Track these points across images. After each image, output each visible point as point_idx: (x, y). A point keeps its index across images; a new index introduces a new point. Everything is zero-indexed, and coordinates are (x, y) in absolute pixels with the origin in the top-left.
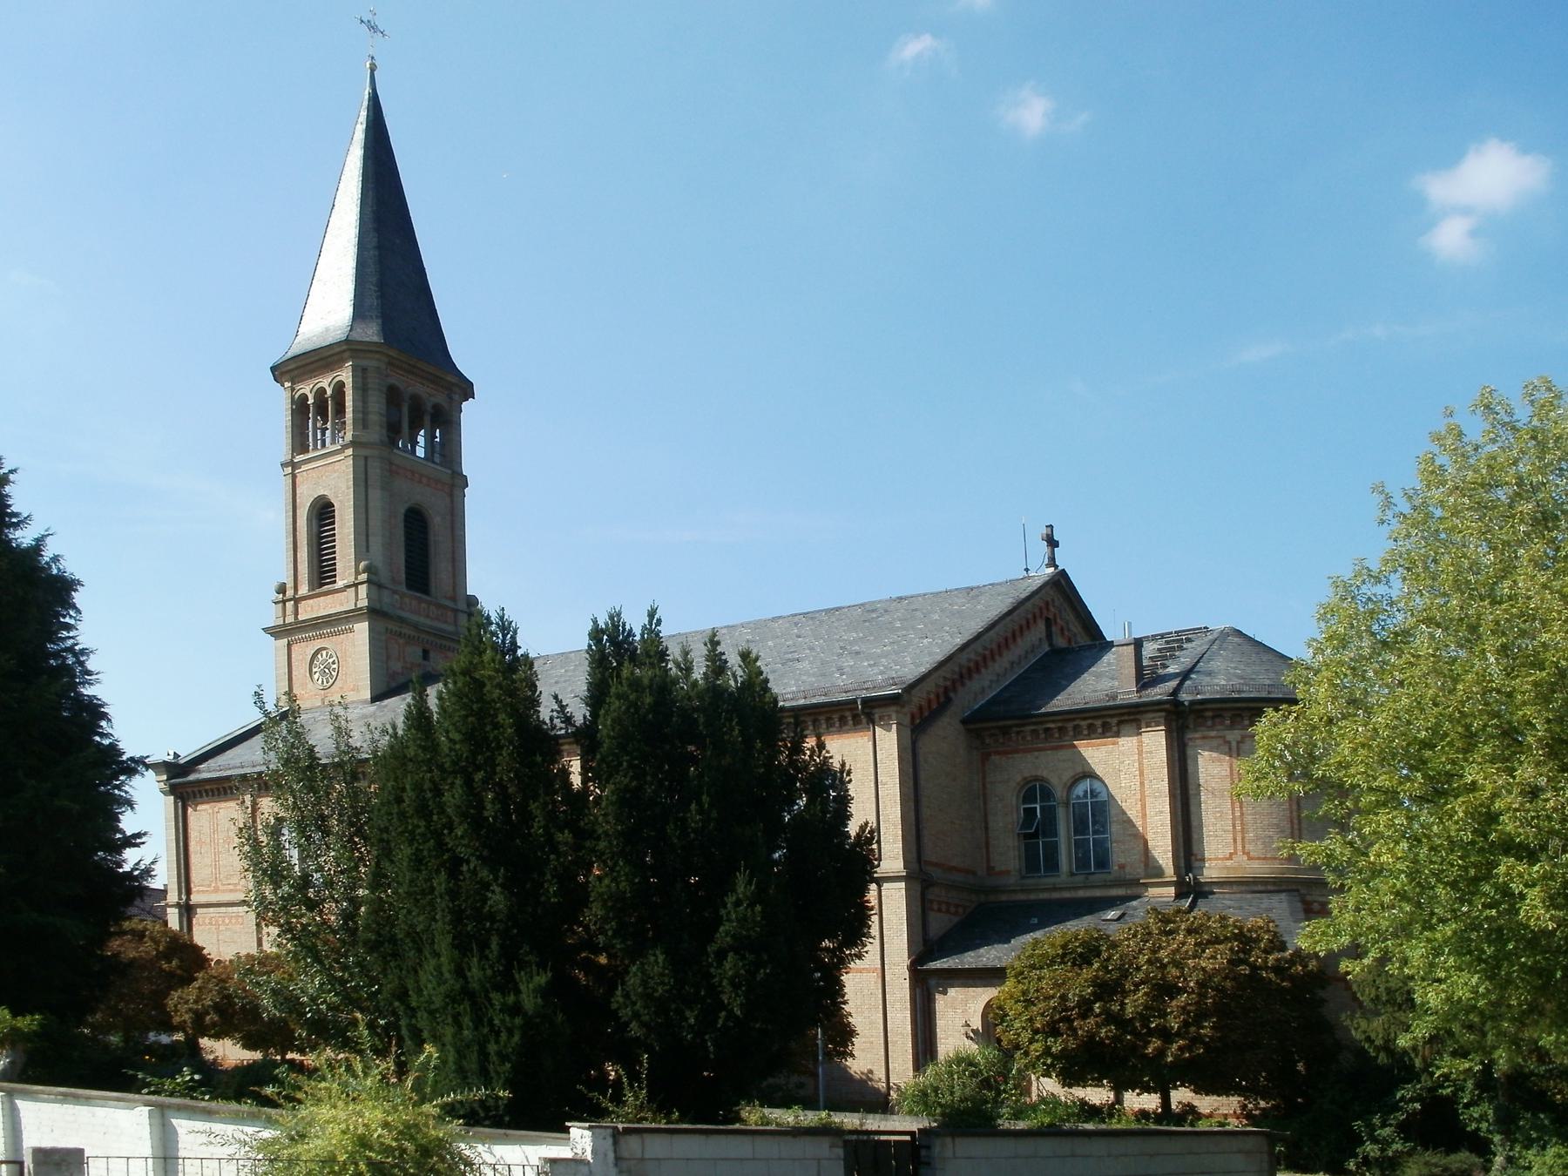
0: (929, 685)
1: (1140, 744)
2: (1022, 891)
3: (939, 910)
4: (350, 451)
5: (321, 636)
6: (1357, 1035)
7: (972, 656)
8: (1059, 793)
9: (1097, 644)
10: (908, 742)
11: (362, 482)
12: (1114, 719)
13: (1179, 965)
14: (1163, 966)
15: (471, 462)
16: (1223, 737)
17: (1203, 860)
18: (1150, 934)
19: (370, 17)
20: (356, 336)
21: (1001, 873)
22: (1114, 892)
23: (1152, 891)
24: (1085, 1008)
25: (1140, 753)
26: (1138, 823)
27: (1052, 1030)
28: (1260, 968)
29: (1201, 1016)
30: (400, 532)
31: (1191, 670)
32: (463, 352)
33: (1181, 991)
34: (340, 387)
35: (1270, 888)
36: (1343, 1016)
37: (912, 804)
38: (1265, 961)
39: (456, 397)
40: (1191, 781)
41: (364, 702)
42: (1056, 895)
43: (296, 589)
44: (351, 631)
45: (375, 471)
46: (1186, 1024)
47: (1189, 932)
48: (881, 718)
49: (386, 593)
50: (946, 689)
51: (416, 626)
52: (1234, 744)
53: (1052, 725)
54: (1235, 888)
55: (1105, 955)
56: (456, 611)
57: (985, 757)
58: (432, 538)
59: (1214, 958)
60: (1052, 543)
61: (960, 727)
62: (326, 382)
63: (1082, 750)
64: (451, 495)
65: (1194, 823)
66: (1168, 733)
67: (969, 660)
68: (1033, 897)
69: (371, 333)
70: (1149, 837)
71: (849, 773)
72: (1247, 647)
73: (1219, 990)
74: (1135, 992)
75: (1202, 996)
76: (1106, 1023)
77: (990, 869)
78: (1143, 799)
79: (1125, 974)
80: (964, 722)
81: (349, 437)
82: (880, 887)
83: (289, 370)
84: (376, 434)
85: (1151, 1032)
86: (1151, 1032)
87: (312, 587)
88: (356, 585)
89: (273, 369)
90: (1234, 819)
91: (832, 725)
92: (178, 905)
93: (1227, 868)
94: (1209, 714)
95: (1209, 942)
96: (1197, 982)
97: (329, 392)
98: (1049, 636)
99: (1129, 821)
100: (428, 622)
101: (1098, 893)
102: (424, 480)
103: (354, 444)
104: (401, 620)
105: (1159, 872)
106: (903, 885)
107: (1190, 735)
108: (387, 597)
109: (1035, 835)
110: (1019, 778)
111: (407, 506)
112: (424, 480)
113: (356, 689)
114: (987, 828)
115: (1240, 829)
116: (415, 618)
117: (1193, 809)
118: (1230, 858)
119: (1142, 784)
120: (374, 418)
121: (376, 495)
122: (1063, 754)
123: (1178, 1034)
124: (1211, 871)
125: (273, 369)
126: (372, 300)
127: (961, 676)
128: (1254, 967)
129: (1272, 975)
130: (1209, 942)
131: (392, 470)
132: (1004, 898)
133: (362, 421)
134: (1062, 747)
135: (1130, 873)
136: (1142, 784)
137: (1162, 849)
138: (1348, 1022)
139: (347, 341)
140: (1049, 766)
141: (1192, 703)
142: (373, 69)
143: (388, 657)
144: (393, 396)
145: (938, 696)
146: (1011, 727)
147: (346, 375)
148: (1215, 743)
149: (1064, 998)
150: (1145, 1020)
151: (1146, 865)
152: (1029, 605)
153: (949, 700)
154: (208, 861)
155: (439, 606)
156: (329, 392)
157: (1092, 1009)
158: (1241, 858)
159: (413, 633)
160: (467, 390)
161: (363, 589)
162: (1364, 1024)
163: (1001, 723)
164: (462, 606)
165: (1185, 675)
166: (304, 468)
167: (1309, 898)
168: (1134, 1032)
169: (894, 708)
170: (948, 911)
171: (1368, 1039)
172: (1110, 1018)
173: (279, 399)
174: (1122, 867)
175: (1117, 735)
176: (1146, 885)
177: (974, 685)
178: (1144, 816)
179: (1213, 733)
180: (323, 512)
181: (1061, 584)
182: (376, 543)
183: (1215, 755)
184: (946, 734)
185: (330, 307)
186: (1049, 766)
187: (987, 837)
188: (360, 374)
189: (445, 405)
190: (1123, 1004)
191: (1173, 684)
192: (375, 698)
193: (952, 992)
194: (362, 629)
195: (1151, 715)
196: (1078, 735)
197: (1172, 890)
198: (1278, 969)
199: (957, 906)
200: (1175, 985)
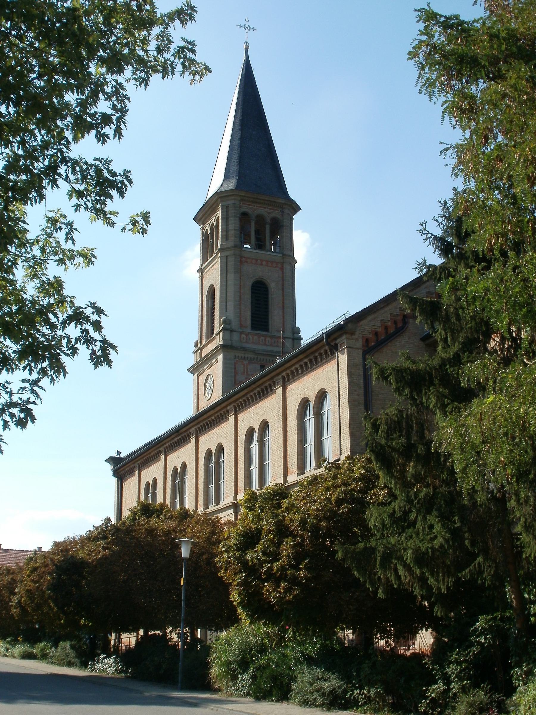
19: (245, 23)
39: (286, 211)
51: (254, 352)
61: (422, 344)
104: (244, 349)
112: (264, 263)
120: (231, 233)
121: (231, 277)
126: (235, 168)
133: (226, 237)
142: (247, 48)
143: (236, 373)
159: (252, 356)
160: (295, 208)
161: (221, 333)
164: (289, 334)
166: (206, 271)
169: (344, 337)
188: (226, 210)
189: (279, 217)
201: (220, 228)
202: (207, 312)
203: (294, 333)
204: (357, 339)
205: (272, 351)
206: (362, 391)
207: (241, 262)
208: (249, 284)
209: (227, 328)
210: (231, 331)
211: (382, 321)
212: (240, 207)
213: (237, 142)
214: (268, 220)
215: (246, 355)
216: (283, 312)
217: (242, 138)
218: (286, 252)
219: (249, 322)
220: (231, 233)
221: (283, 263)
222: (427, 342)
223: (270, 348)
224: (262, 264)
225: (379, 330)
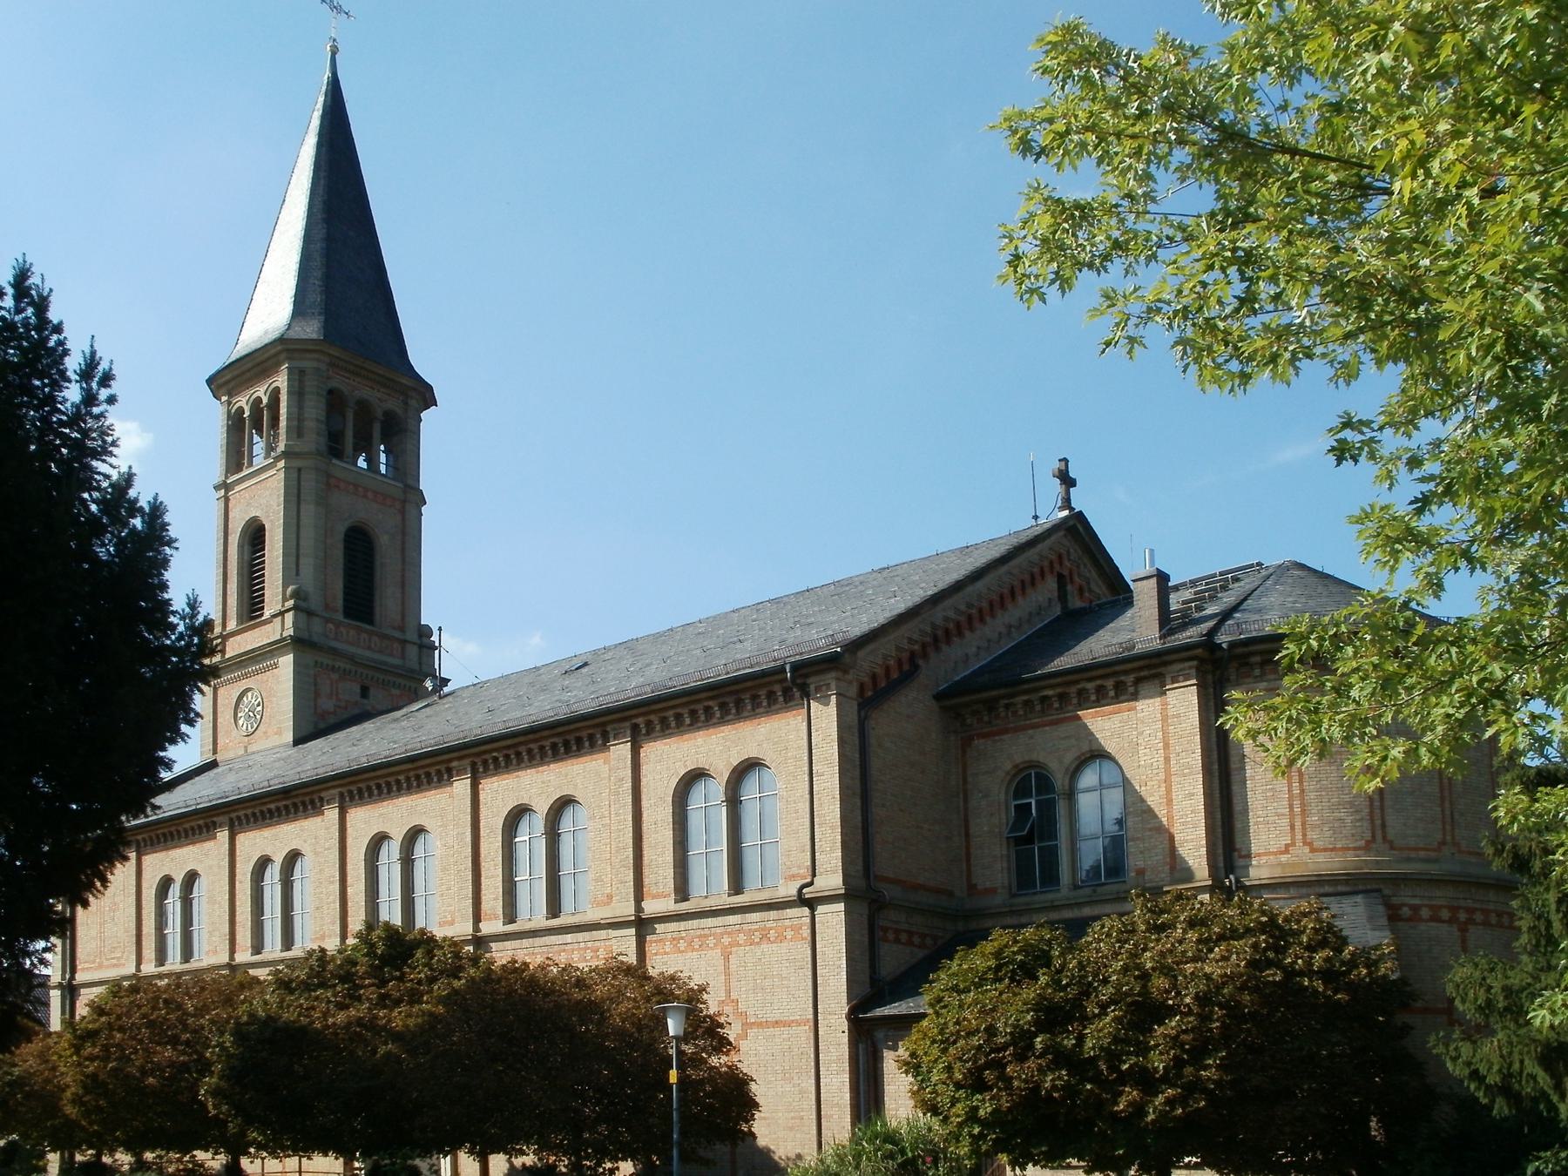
0: (887, 646)
3: (897, 941)
4: (282, 464)
5: (246, 676)
6: (1456, 1070)
7: (951, 614)
8: (1060, 781)
9: (1118, 594)
10: (853, 718)
11: (294, 497)
12: (1134, 676)
13: (1165, 970)
14: (1145, 977)
15: (429, 479)
17: (1249, 856)
18: (1133, 931)
20: (292, 334)
24: (1022, 1042)
26: (1161, 812)
27: (976, 1083)
28: (1301, 973)
29: (1198, 1054)
30: (338, 553)
31: (1235, 608)
32: (425, 353)
33: (1172, 1011)
34: (275, 394)
35: (1341, 888)
36: (1432, 1039)
38: (1309, 963)
39: (413, 403)
41: (286, 745)
43: (224, 625)
44: (276, 666)
45: (310, 482)
46: (1178, 1063)
47: (1192, 924)
48: (818, 689)
49: (316, 620)
50: (913, 655)
51: (351, 658)
53: (1050, 693)
54: (1293, 892)
55: (1057, 963)
56: (405, 642)
57: (966, 743)
58: (378, 561)
59: (1225, 959)
60: (1067, 480)
62: (261, 392)
64: (403, 512)
65: (1237, 808)
66: (1201, 687)
67: (947, 619)
69: (311, 330)
70: (1175, 831)
71: (106, 380)
72: (1313, 580)
73: (1233, 1009)
74: (1099, 1016)
75: (1205, 1018)
76: (1056, 1064)
77: (972, 887)
78: (1167, 781)
79: (1086, 991)
80: (938, 697)
81: (281, 447)
82: (813, 910)
83: (225, 381)
84: (313, 440)
85: (1123, 1078)
86: (1123, 1078)
87: (240, 620)
88: (282, 614)
89: (210, 382)
90: (1291, 799)
91: (759, 705)
92: (60, 986)
93: (1280, 864)
94: (1257, 659)
95: (1222, 938)
96: (1197, 997)
97: (265, 400)
98: (1062, 596)
100: (368, 654)
102: (370, 494)
103: (286, 455)
104: (334, 652)
105: (1188, 875)
106: (841, 906)
108: (317, 626)
109: (1029, 839)
110: (1008, 766)
111: (347, 524)
112: (370, 494)
113: (279, 733)
114: (967, 835)
115: (1300, 810)
116: (352, 649)
117: (1235, 788)
118: (1286, 851)
119: (1167, 760)
120: (310, 424)
121: (309, 511)
122: (1064, 730)
123: (1166, 1080)
124: (1259, 871)
125: (210, 382)
126: (316, 297)
127: (936, 639)
128: (1290, 973)
129: (1319, 985)
130: (1222, 938)
131: (329, 483)
133: (296, 430)
136: (1167, 760)
137: (1193, 847)
138: (1440, 1049)
139: (281, 340)
140: (1044, 746)
141: (1232, 645)
143: (317, 694)
144: (335, 401)
145: (900, 662)
147: (281, 380)
149: (991, 1031)
150: (1113, 1058)
151: (1173, 868)
152: (1032, 554)
153: (915, 668)
154: (94, 933)
155: (384, 637)
156: (265, 400)
157: (1031, 1046)
159: (348, 667)
160: (426, 396)
161: (289, 617)
162: (1466, 1049)
163: (985, 695)
165: (1226, 615)
166: (237, 488)
167: (1395, 900)
168: (1097, 1079)
169: (833, 674)
170: (910, 943)
171: (1475, 1075)
172: (1061, 1058)
173: (213, 416)
175: (1135, 697)
177: (954, 651)
178: (1170, 802)
180: (255, 535)
181: (1077, 530)
182: (308, 565)
184: (910, 714)
185: (271, 308)
186: (1044, 746)
187: (968, 848)
188: (297, 377)
189: (399, 411)
190: (1081, 1039)
191: (1211, 624)
192: (299, 741)
194: (287, 662)
196: (1084, 701)
198: (1328, 975)
200: (1163, 1004)
201: (283, 410)
202: (240, 569)
203: (420, 636)
204: (850, 682)
205: (385, 664)
206: (857, 773)
207: (328, 484)
208: (341, 529)
209: (302, 606)
210: (310, 613)
211: (885, 657)
212: (329, 378)
213: (318, 246)
214: (379, 414)
215: (337, 664)
216: (403, 593)
217: (329, 239)
218: (410, 482)
219: (340, 603)
220: (310, 424)
221: (404, 501)
222: (947, 703)
223: (376, 656)
224: (365, 496)
225: (879, 670)
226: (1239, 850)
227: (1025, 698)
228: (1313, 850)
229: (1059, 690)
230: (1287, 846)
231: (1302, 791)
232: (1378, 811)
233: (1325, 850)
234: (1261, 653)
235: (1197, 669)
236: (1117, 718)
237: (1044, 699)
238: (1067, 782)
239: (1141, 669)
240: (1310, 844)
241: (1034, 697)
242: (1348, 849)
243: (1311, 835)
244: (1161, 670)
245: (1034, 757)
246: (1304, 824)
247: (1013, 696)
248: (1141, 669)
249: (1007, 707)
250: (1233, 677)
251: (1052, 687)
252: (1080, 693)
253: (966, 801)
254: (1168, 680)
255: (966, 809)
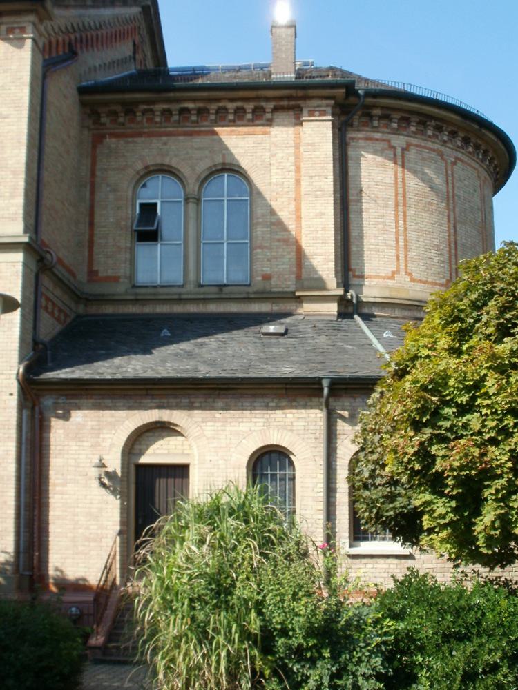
1: (298, 136)
2: (136, 301)
16: (389, 141)
17: (362, 277)
21: (109, 279)
22: (256, 308)
23: (308, 308)
25: (297, 146)
26: (292, 227)
37: (36, 152)
40: (351, 186)
42: (178, 309)
52: (399, 150)
53: (191, 105)
54: (397, 313)
57: (98, 140)
63: (224, 138)
68: (148, 309)
70: (304, 243)
77: (92, 274)
78: (298, 199)
80: (82, 91)
90: (397, 233)
93: (387, 287)
99: (280, 224)
101: (234, 308)
105: (320, 284)
107: (351, 134)
114: (91, 224)
117: (352, 216)
118: (392, 278)
119: (298, 182)
122: (197, 141)
132: (109, 309)
134: (199, 133)
135: (276, 285)
136: (298, 182)
137: (322, 256)
146: (137, 103)
148: (379, 146)
151: (299, 277)
158: (402, 279)
163: (128, 96)
169: (32, 18)
174: (267, 278)
175: (270, 123)
176: (300, 300)
178: (299, 218)
179: (378, 135)
183: (379, 159)
187: (92, 235)
193: (78, 416)
195: (315, 102)
196: (222, 117)
197: (333, 308)
199: (60, 310)
222: (87, 98)
226: (354, 271)
227: (165, 106)
228: (412, 280)
229: (200, 105)
230: (393, 273)
231: (406, 229)
232: (453, 257)
233: (420, 281)
234: (383, 108)
235: (333, 107)
236: (251, 139)
237: (183, 111)
238: (196, 189)
239: (281, 98)
240: (410, 274)
241: (175, 107)
242: (436, 284)
243: (411, 267)
244: (301, 103)
245: (167, 161)
246: (406, 256)
247: (153, 102)
248: (281, 98)
249: (144, 112)
250: (356, 123)
251: (194, 100)
252: (218, 111)
253: (92, 193)
254: (305, 112)
255: (92, 201)
